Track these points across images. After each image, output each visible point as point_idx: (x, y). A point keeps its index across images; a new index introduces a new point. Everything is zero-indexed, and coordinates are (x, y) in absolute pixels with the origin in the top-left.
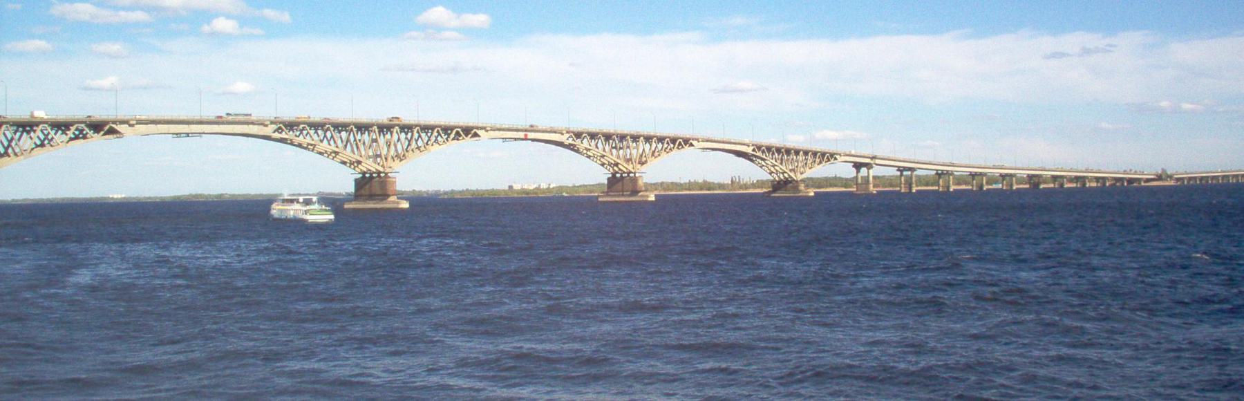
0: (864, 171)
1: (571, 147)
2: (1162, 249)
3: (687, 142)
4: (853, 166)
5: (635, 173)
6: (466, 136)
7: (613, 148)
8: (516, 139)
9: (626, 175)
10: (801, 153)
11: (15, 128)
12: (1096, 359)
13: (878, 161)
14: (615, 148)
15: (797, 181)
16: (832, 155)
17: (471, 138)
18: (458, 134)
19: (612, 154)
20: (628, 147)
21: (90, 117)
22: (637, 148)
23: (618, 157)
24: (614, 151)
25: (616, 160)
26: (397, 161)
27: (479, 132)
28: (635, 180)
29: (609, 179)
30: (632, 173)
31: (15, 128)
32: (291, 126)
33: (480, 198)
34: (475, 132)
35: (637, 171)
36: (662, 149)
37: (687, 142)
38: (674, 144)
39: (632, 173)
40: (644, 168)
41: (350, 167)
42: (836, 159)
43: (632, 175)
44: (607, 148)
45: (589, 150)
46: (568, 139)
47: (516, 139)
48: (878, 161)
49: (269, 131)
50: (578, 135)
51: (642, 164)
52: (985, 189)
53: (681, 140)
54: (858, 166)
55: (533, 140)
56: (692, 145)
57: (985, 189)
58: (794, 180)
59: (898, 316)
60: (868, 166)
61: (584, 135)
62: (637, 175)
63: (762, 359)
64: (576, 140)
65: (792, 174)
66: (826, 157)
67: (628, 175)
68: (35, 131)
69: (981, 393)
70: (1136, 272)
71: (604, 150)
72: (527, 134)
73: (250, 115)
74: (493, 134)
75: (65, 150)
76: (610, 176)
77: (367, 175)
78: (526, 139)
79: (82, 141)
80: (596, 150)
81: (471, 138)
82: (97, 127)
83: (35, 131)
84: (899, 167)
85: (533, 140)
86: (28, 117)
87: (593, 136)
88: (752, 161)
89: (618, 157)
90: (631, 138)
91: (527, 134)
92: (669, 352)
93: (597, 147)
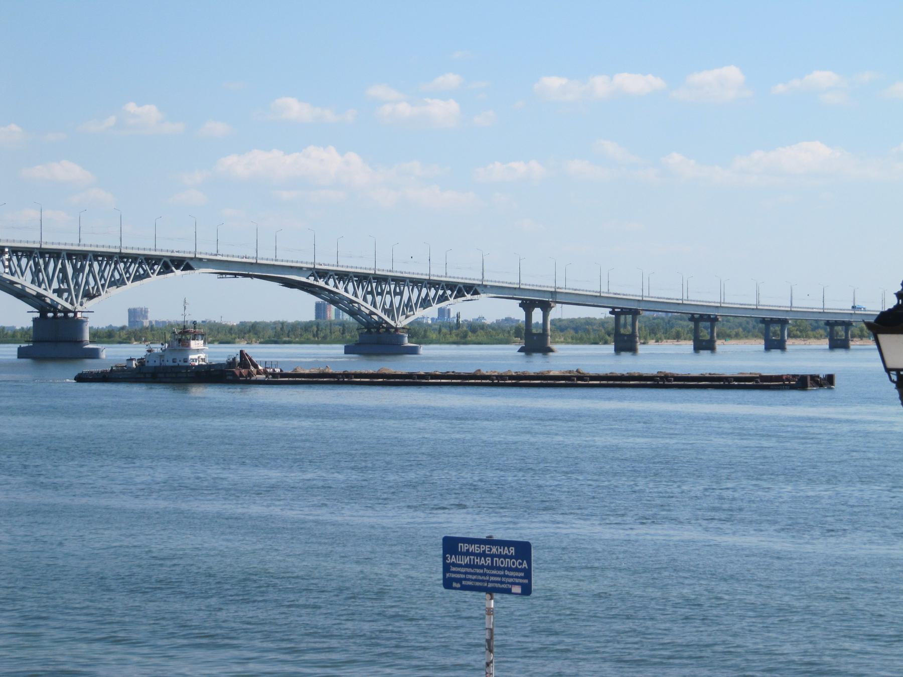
0: (537, 315)
2: (812, 444)
4: (521, 305)
5: (75, 313)
7: (369, 293)
14: (371, 293)
15: (396, 329)
20: (389, 293)
22: (401, 294)
24: (369, 297)
28: (78, 324)
29: (35, 320)
34: (476, 289)
35: (79, 308)
40: (89, 305)
43: (71, 315)
44: (360, 292)
51: (89, 296)
53: (461, 286)
54: (528, 306)
58: (392, 327)
61: (331, 273)
62: (79, 315)
63: (883, 621)
69: (339, 643)
71: (356, 295)
76: (38, 315)
86: (328, 317)
92: (315, 602)
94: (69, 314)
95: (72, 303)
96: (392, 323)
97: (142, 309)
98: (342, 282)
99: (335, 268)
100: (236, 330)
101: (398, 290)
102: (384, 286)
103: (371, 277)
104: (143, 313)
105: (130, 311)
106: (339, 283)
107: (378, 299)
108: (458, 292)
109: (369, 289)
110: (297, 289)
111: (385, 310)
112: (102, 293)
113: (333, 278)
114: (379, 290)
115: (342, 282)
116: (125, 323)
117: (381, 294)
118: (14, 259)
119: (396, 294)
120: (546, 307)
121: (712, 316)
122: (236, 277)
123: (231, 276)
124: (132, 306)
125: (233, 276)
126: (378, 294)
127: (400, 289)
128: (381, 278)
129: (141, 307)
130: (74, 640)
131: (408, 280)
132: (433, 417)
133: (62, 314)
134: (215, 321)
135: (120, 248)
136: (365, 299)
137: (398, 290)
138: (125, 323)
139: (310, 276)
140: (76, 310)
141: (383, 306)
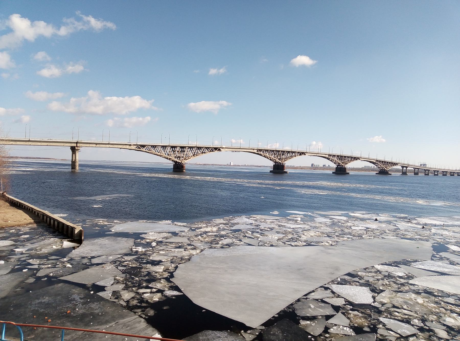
0: (405, 168)
1: (328, 159)
3: (358, 158)
6: (303, 154)
8: (314, 156)
10: (347, 157)
11: (161, 147)
13: (409, 166)
16: (397, 164)
18: (300, 154)
21: (424, 165)
27: (306, 154)
30: (343, 166)
31: (161, 147)
32: (261, 150)
37: (358, 158)
39: (343, 166)
40: (347, 165)
41: (272, 161)
42: (398, 165)
43: (343, 167)
47: (314, 156)
48: (409, 166)
49: (255, 151)
50: (330, 155)
54: (403, 167)
55: (318, 156)
56: (359, 159)
59: (456, 244)
60: (407, 167)
64: (260, 152)
65: (385, 168)
66: (396, 164)
67: (342, 167)
68: (156, 148)
72: (317, 155)
74: (309, 154)
75: (299, 158)
77: (277, 164)
79: (294, 158)
82: (216, 149)
83: (156, 148)
84: (414, 168)
85: (318, 156)
87: (334, 156)
88: (395, 311)
91: (317, 155)
120: (407, 167)
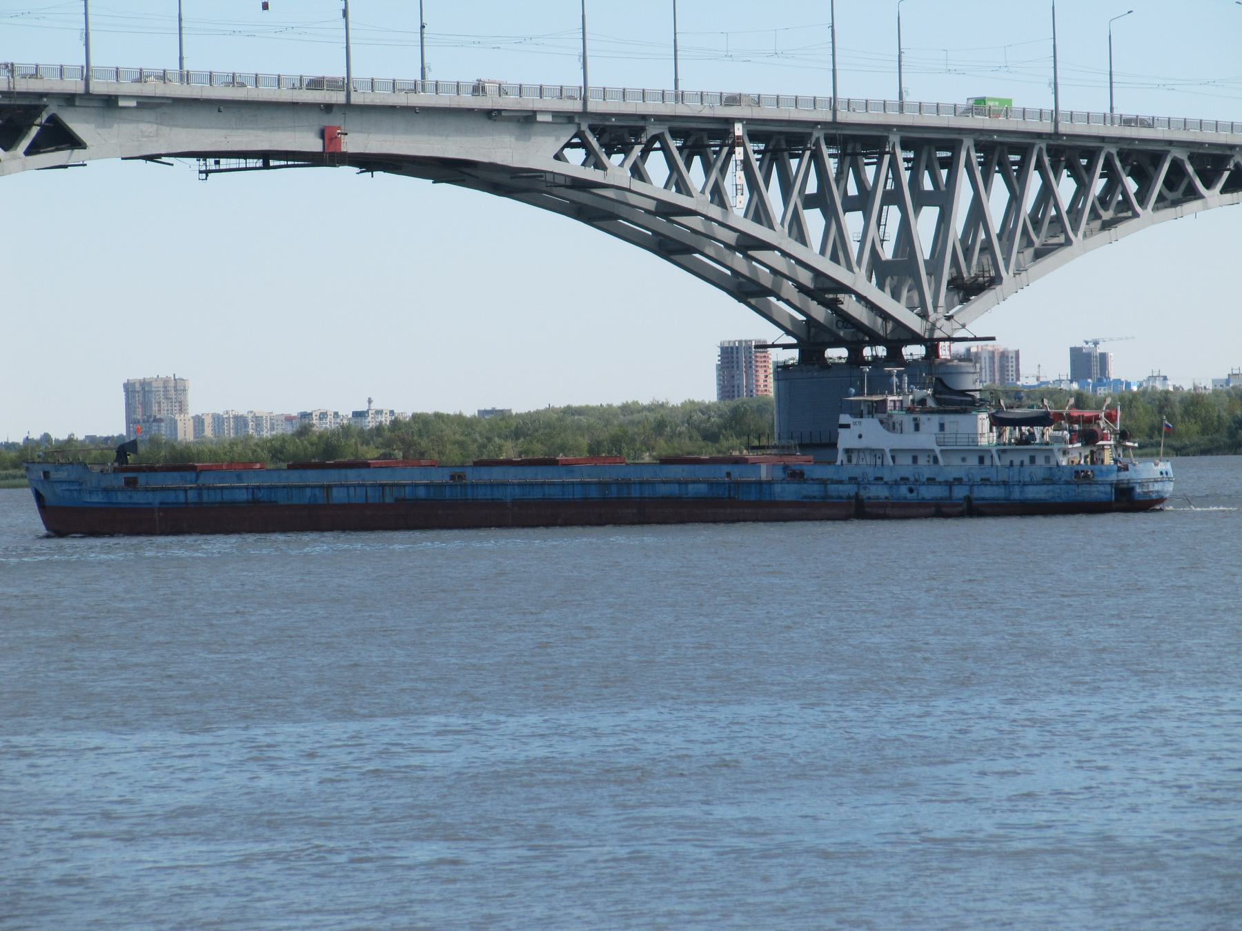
7: (810, 202)
8: (267, 158)
9: (881, 351)
12: (1195, 827)
17: (28, 152)
19: (802, 239)
20: (893, 197)
22: (943, 199)
23: (837, 248)
25: (826, 266)
26: (1061, 453)
27: (79, 127)
30: (915, 339)
33: (220, 503)
34: (53, 119)
35: (944, 329)
36: (1074, 211)
38: (1145, 182)
39: (915, 339)
45: (747, 244)
46: (559, 157)
51: (966, 289)
52: (1086, 160)
53: (1182, 155)
55: (369, 163)
57: (1086, 160)
61: (652, 131)
62: (945, 351)
70: (776, 458)
73: (993, 339)
78: (330, 157)
80: (715, 212)
81: (28, 152)
89: (837, 248)
90: (979, 147)
93: (717, 195)
94: (885, 354)
95: (924, 315)
96: (914, 322)
97: (166, 381)
98: (697, 160)
99: (668, 109)
100: (315, 439)
101: (928, 185)
102: (870, 172)
103: (818, 134)
104: (172, 393)
105: (129, 388)
106: (688, 165)
107: (853, 222)
108: (1169, 184)
109: (812, 187)
110: (900, 215)
111: (879, 269)
112: (1003, 273)
113: (665, 149)
114: (852, 190)
115: (697, 160)
116: (706, 390)
117: (862, 202)
118: (696, 174)
119: (921, 199)
121: (888, 187)
122: (266, 166)
123: (242, 163)
124: (137, 375)
125: (260, 163)
126: (851, 205)
127: (935, 179)
128: (855, 138)
129: (163, 376)
130: (1189, 893)
131: (895, 138)
132: (464, 731)
133: (867, 352)
134: (47, 437)
135: (833, 104)
136: (798, 231)
137: (928, 185)
138: (706, 390)
139: (569, 145)
140: (938, 334)
141: (874, 252)
